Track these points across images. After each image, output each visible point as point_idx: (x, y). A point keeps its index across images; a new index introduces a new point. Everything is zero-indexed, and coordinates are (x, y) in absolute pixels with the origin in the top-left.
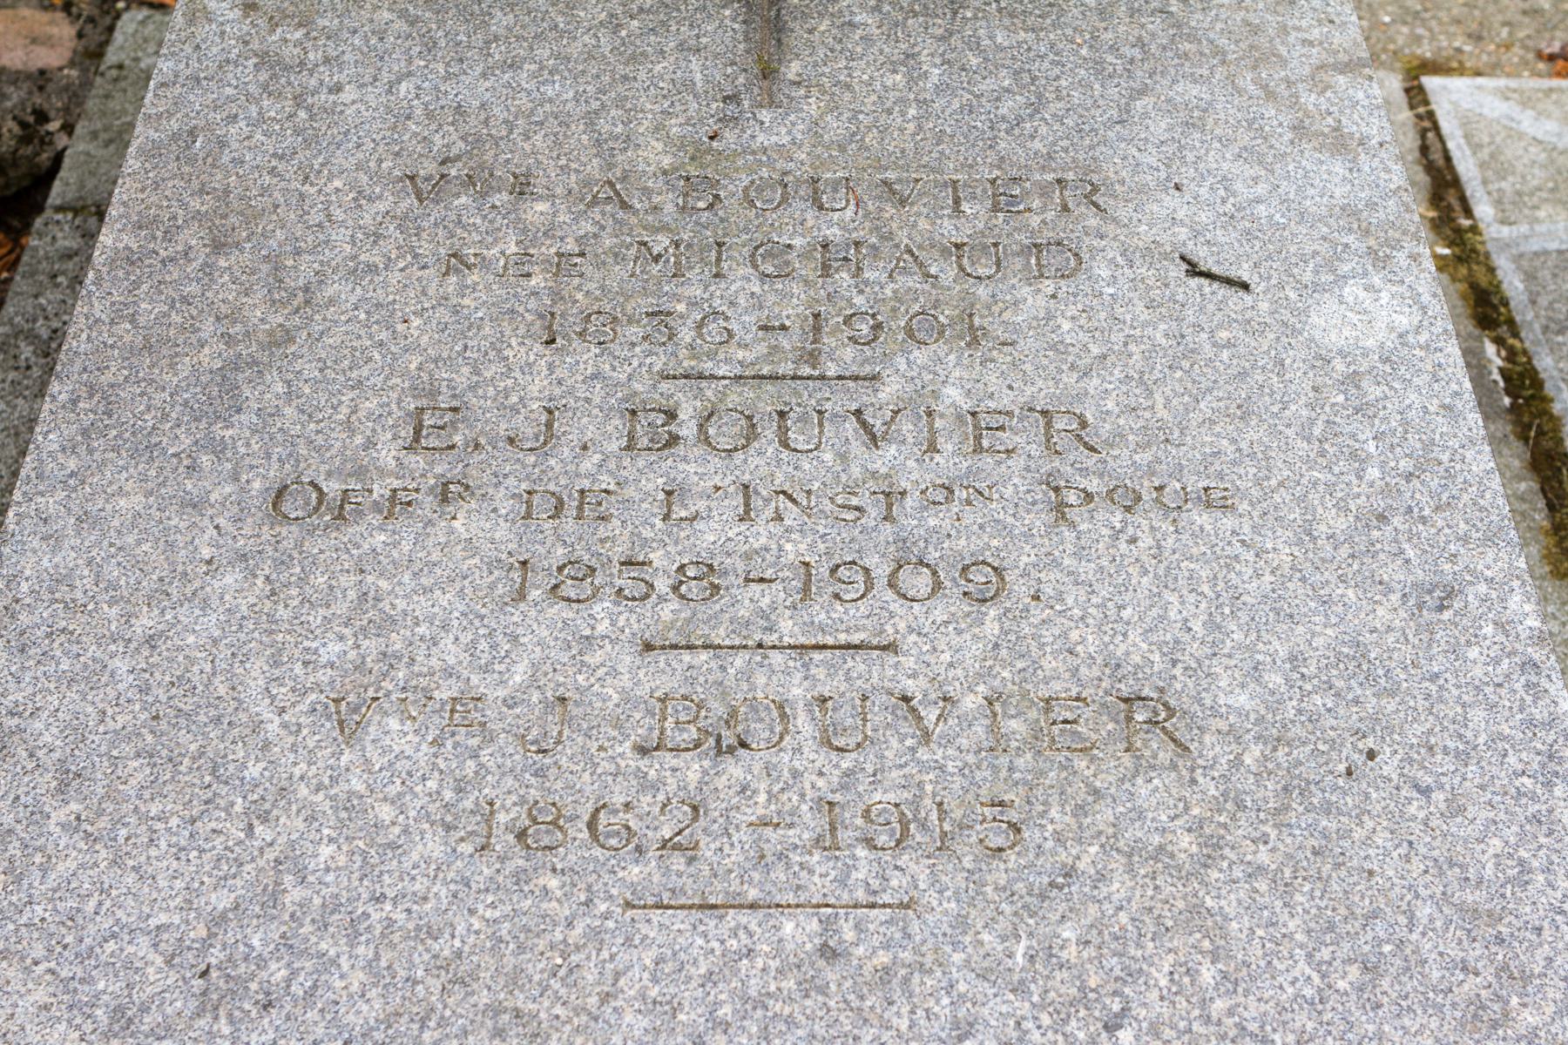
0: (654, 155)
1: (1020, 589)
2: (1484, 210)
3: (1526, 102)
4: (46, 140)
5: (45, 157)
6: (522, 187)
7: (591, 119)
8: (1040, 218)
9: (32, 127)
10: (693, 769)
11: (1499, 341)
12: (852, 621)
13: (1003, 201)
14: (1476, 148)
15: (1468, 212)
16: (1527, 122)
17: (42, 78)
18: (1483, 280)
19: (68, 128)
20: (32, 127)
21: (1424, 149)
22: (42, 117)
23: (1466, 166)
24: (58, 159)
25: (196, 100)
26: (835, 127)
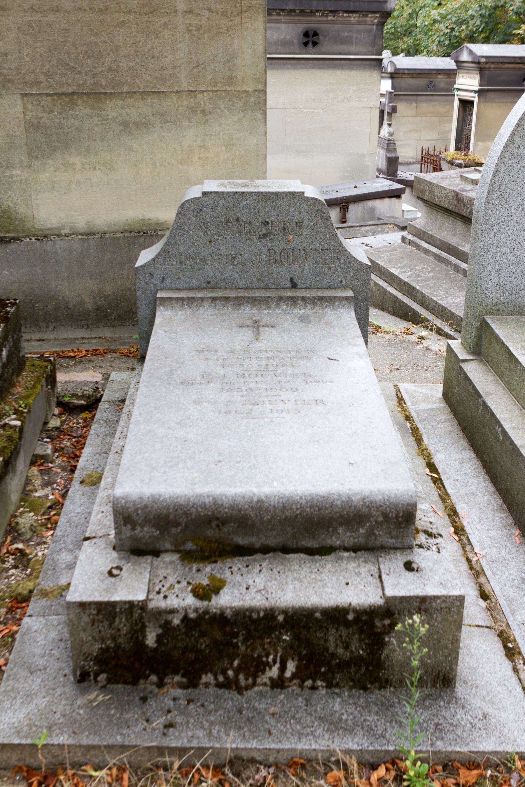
0: (238, 348)
1: (300, 390)
2: (409, 403)
3: (419, 387)
4: (99, 392)
5: (99, 395)
6: (216, 351)
7: (227, 344)
8: (304, 354)
9: (96, 390)
10: (251, 407)
11: (410, 423)
12: (275, 393)
13: (297, 352)
14: (408, 394)
15: (405, 404)
16: (419, 390)
17: (96, 382)
18: (407, 414)
19: (104, 391)
20: (96, 390)
21: (397, 395)
22: (98, 388)
23: (405, 397)
24: (102, 396)
25: (159, 342)
26: (269, 344)
